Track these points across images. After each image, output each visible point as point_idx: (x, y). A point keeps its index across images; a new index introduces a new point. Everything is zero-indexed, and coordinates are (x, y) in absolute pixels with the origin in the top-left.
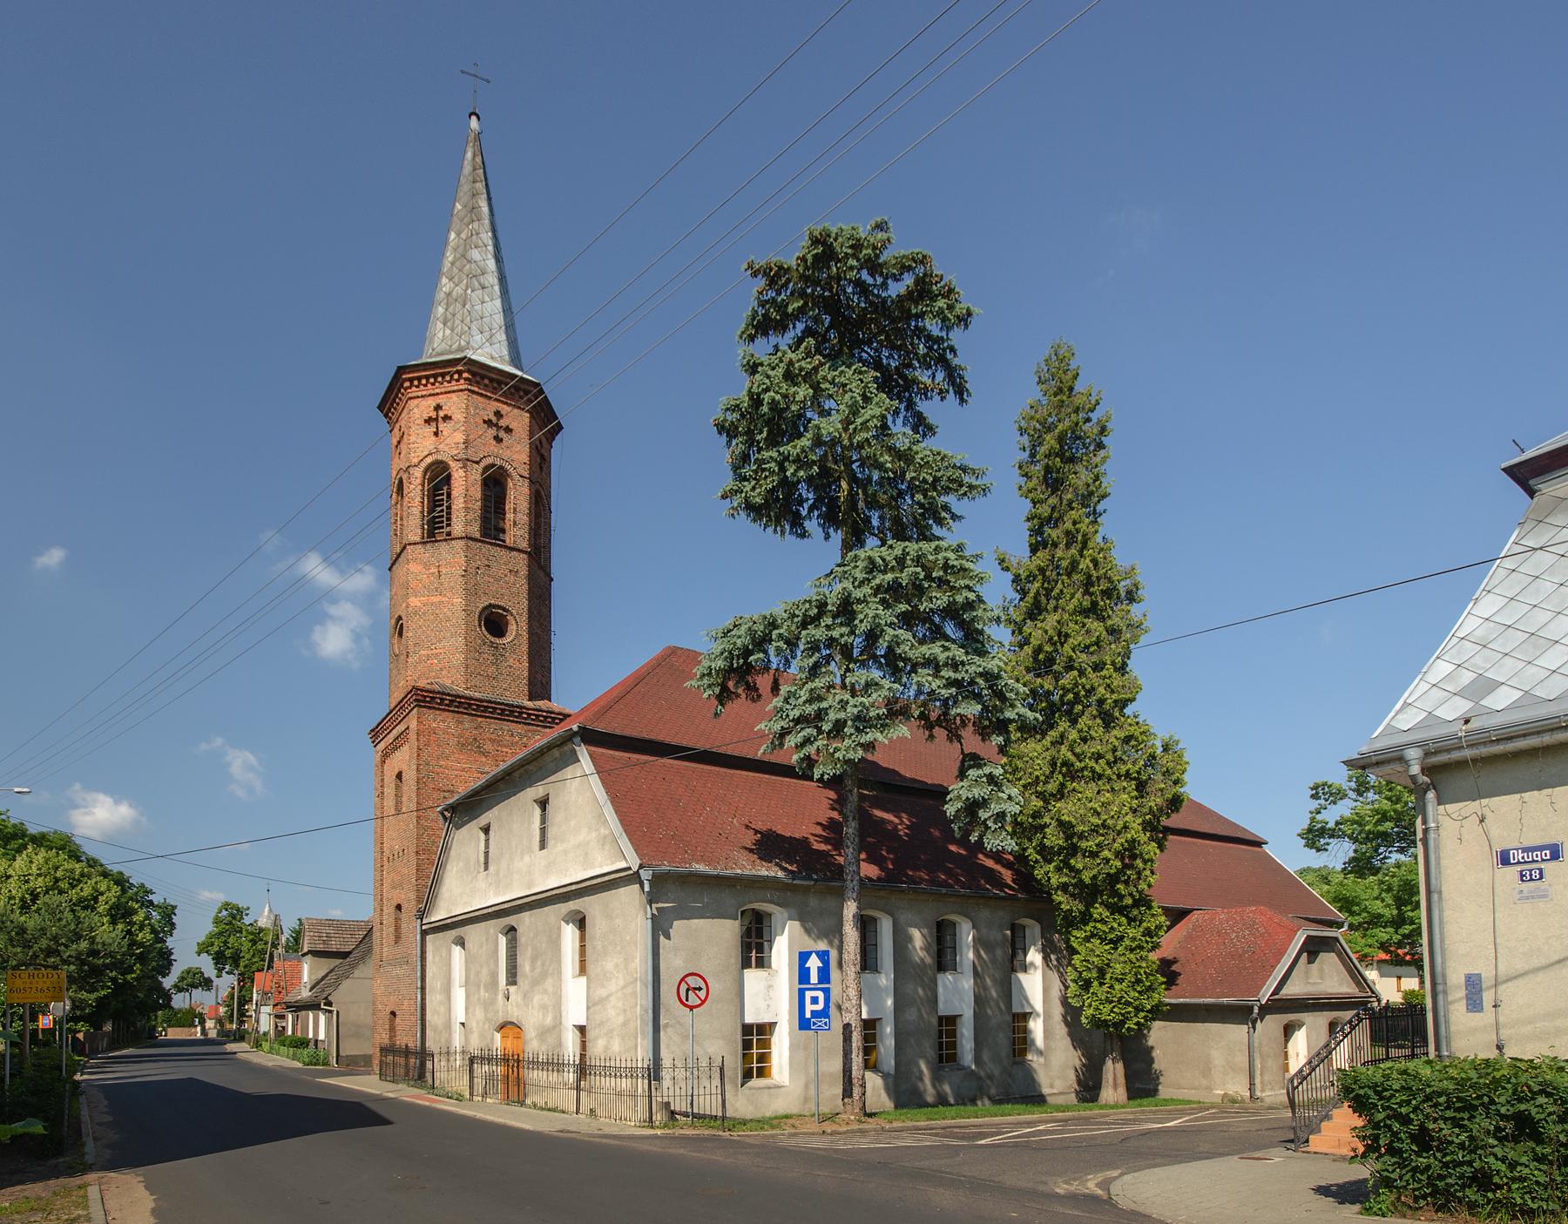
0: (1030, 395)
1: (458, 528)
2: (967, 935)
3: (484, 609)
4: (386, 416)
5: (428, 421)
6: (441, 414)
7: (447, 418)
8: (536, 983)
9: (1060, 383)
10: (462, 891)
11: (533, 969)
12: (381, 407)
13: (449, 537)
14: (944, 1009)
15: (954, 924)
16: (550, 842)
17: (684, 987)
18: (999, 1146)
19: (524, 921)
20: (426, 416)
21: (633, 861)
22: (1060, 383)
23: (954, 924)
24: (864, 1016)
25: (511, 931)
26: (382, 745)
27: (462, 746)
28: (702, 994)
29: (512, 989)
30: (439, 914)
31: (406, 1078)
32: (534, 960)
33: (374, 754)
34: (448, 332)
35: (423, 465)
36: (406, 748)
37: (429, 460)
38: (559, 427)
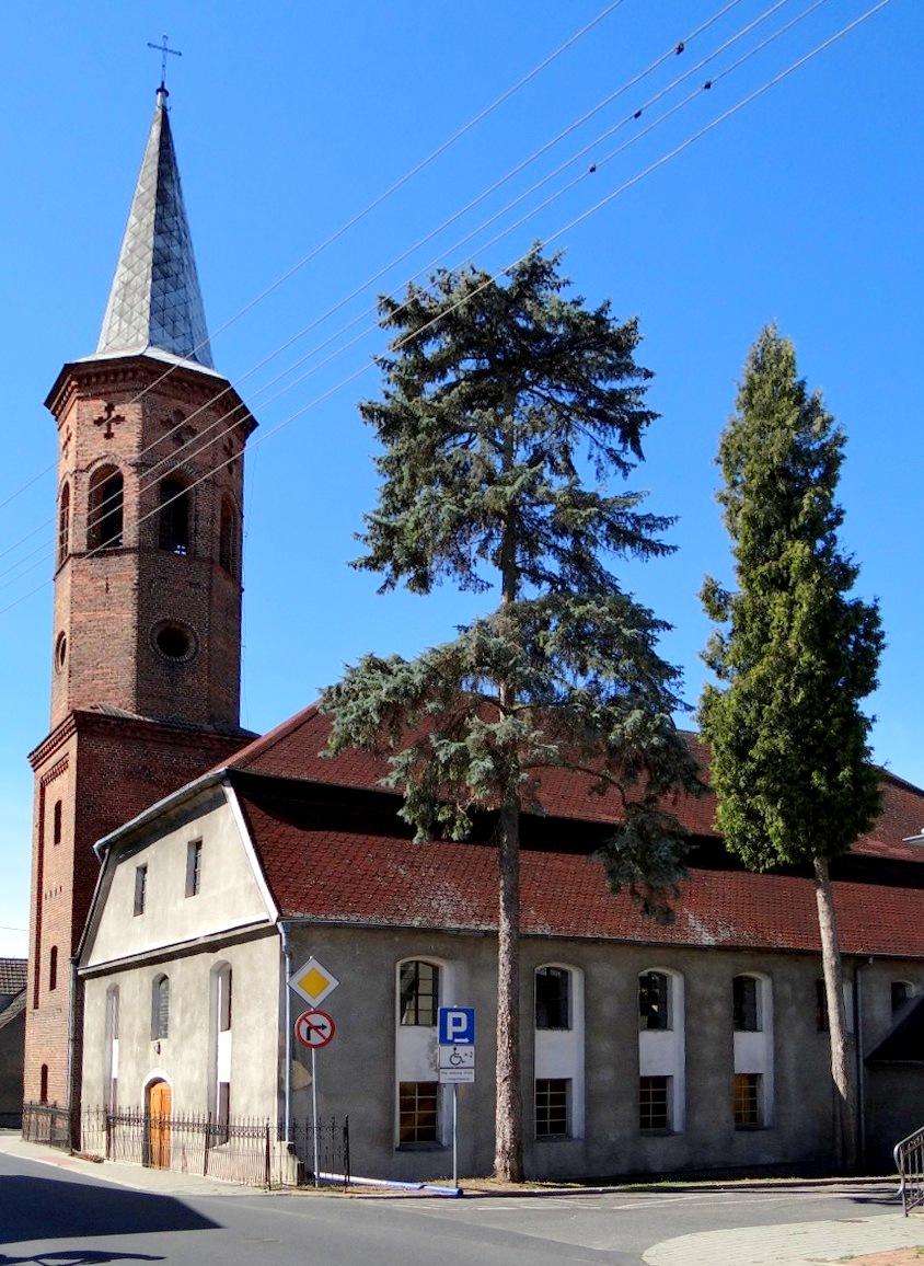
0: (724, 413)
1: (129, 534)
2: (765, 989)
3: (159, 624)
4: (53, 413)
5: (99, 422)
6: (114, 414)
7: (119, 419)
8: (185, 1037)
9: (776, 391)
10: (117, 936)
11: (183, 1021)
12: (48, 403)
13: (119, 550)
14: (648, 1069)
15: (753, 981)
16: (202, 887)
17: (304, 1026)
18: (629, 1210)
19: (177, 970)
20: (96, 417)
21: (272, 913)
22: (776, 391)
23: (753, 981)
24: (116, 1042)
25: (226, 973)
26: (42, 771)
27: (129, 775)
28: (327, 1033)
29: (163, 1042)
30: (96, 959)
31: (53, 1142)
32: (184, 1012)
33: (30, 781)
34: (124, 325)
35: (93, 469)
36: (65, 775)
37: (99, 464)
38: (252, 424)
